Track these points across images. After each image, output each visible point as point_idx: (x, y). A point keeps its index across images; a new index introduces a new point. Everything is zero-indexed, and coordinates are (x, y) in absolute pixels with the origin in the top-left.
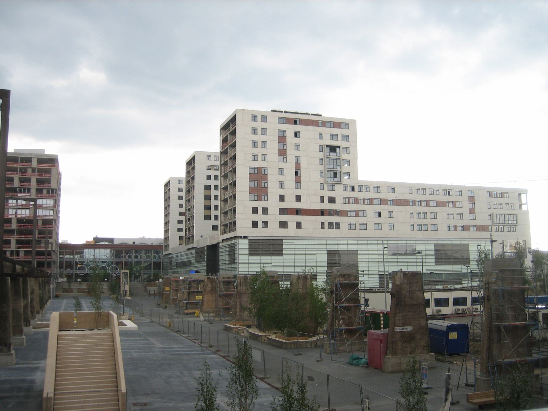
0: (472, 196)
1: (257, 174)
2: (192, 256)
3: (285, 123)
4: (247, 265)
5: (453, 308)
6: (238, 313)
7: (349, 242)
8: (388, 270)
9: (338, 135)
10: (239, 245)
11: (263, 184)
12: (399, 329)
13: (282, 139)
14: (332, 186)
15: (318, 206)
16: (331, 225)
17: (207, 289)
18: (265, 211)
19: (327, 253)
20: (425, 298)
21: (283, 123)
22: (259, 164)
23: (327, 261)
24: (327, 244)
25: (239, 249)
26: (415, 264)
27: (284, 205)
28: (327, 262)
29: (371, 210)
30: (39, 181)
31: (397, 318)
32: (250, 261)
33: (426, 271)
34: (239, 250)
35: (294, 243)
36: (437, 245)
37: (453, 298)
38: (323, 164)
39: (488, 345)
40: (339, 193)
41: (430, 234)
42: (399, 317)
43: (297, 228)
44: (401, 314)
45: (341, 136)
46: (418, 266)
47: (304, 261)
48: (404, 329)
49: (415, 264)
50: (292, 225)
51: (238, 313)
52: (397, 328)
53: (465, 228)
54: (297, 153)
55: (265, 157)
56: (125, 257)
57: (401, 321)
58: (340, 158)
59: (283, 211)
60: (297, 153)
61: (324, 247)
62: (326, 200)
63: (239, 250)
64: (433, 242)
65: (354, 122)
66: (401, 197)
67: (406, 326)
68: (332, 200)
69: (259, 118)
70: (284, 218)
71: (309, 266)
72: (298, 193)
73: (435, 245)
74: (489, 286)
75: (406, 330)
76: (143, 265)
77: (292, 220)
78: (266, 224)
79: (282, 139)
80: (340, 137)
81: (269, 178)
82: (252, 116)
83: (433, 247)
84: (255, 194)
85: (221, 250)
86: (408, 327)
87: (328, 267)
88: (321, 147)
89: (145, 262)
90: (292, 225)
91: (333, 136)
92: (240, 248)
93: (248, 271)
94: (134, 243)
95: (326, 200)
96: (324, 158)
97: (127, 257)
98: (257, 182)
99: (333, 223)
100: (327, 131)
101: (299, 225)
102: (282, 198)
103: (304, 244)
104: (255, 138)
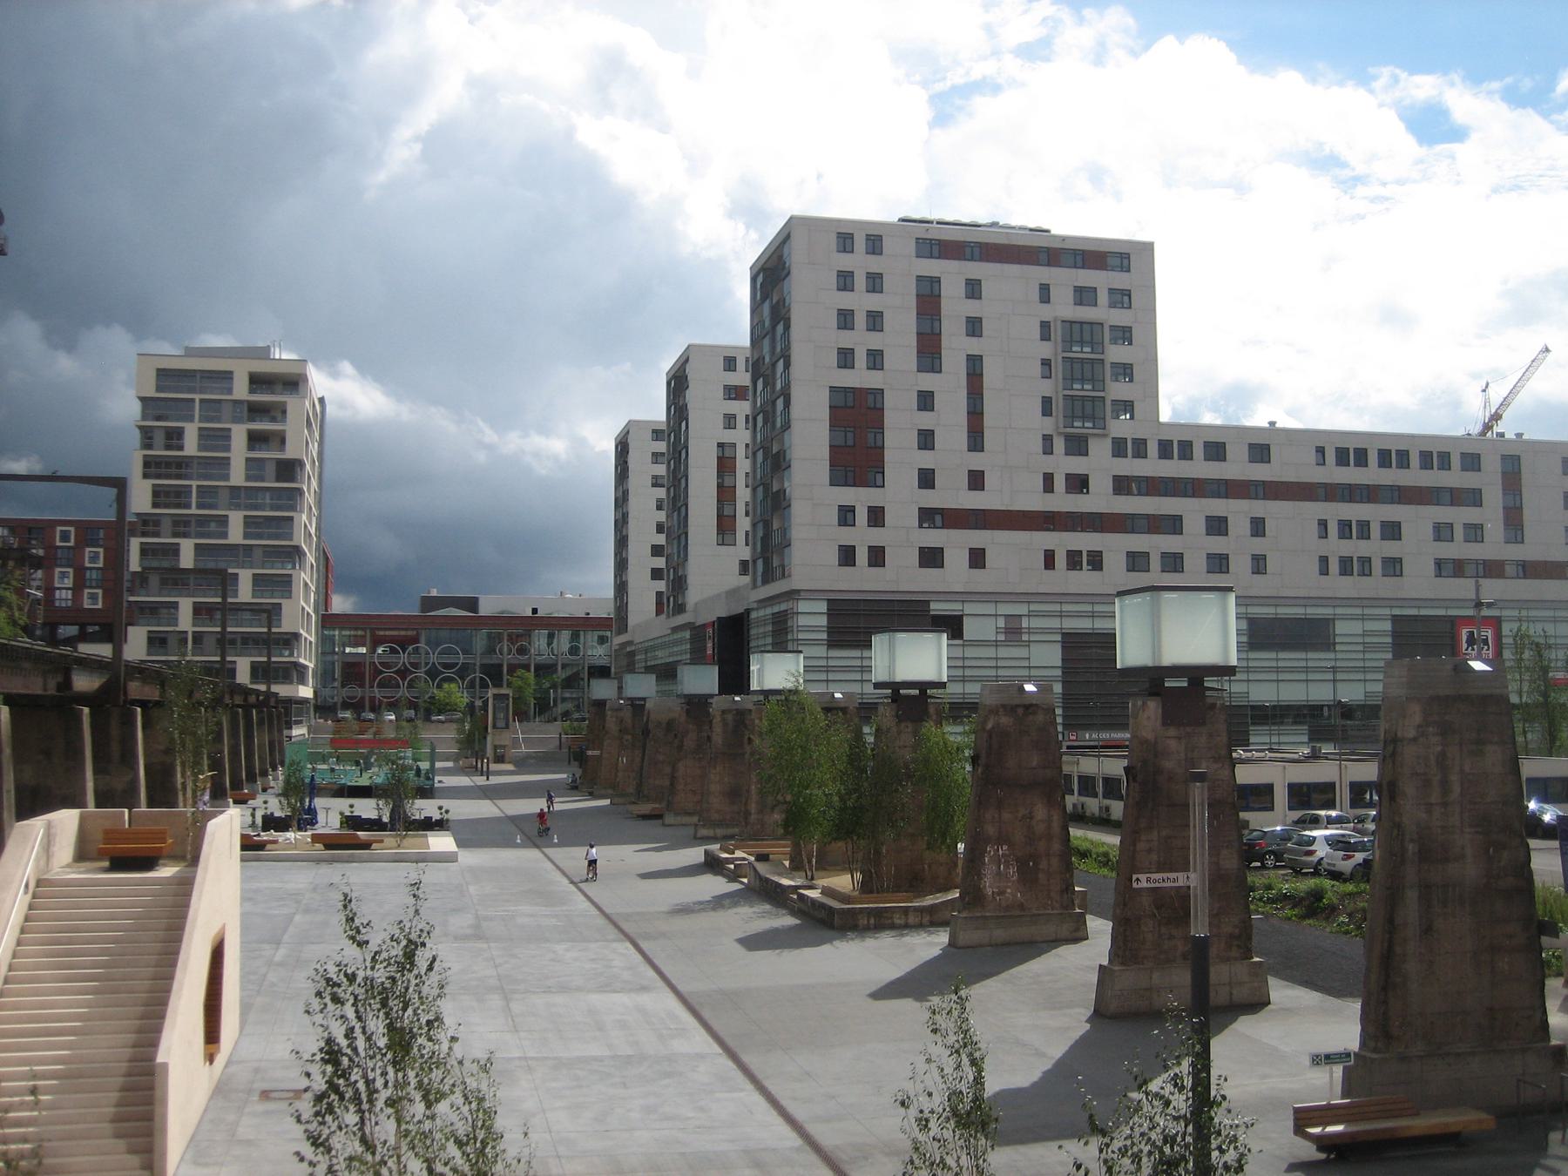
0: (846, 407)
1: (853, 407)
2: (684, 647)
3: (937, 255)
4: (823, 676)
5: (1286, 816)
6: (753, 817)
7: (1066, 608)
8: (1248, 693)
9: (1098, 290)
10: (800, 616)
11: (871, 436)
12: (1148, 880)
13: (929, 300)
14: (1077, 446)
15: (1035, 501)
16: (1074, 560)
17: (685, 743)
18: (877, 516)
19: (1063, 642)
20: (1238, 782)
21: (931, 257)
22: (860, 377)
23: (1063, 664)
24: (1061, 615)
25: (800, 629)
26: (1303, 676)
27: (933, 499)
28: (1063, 668)
29: (1195, 511)
30: (255, 439)
31: (1141, 846)
32: (831, 663)
33: (1366, 696)
34: (798, 631)
35: (963, 610)
36: (1416, 620)
37: (1350, 783)
38: (1050, 377)
39: (1386, 944)
40: (1100, 464)
41: (1377, 585)
42: (1148, 841)
43: (971, 567)
44: (1156, 833)
45: (1106, 292)
46: (1281, 684)
47: (993, 663)
48: (1164, 880)
49: (1303, 676)
50: (957, 558)
51: (753, 817)
52: (1140, 876)
53: (1493, 569)
54: (974, 346)
55: (876, 359)
56: (510, 651)
57: (1154, 857)
58: (1103, 360)
59: (928, 517)
60: (974, 346)
61: (1054, 623)
62: (1060, 483)
63: (798, 631)
64: (1387, 611)
65: (1148, 248)
66: (1290, 476)
67: (1171, 870)
68: (1079, 484)
69: (860, 244)
70: (934, 537)
71: (974, 679)
72: (977, 461)
73: (1396, 619)
74: (1394, 748)
75: (1173, 885)
76: (561, 674)
77: (956, 543)
78: (877, 556)
79: (929, 300)
80: (1103, 297)
81: (889, 418)
82: (838, 237)
83: (1388, 626)
84: (846, 467)
85: (753, 632)
86: (1177, 874)
87: (1063, 682)
88: (1045, 327)
89: (564, 666)
90: (957, 558)
91: (1084, 295)
92: (1033, 628)
93: (962, 692)
94: (536, 613)
95: (1060, 483)
96: (1056, 359)
97: (514, 651)
98: (854, 432)
99: (1081, 551)
100: (1064, 279)
101: (977, 558)
102: (927, 479)
103: (994, 613)
104: (846, 300)
